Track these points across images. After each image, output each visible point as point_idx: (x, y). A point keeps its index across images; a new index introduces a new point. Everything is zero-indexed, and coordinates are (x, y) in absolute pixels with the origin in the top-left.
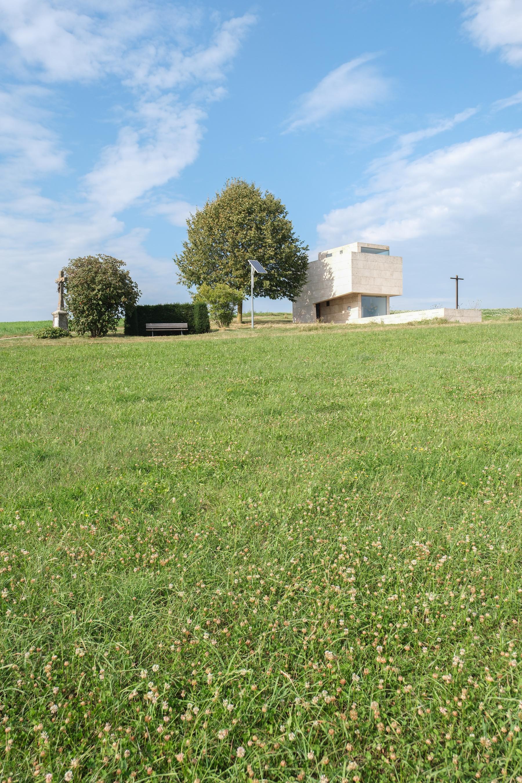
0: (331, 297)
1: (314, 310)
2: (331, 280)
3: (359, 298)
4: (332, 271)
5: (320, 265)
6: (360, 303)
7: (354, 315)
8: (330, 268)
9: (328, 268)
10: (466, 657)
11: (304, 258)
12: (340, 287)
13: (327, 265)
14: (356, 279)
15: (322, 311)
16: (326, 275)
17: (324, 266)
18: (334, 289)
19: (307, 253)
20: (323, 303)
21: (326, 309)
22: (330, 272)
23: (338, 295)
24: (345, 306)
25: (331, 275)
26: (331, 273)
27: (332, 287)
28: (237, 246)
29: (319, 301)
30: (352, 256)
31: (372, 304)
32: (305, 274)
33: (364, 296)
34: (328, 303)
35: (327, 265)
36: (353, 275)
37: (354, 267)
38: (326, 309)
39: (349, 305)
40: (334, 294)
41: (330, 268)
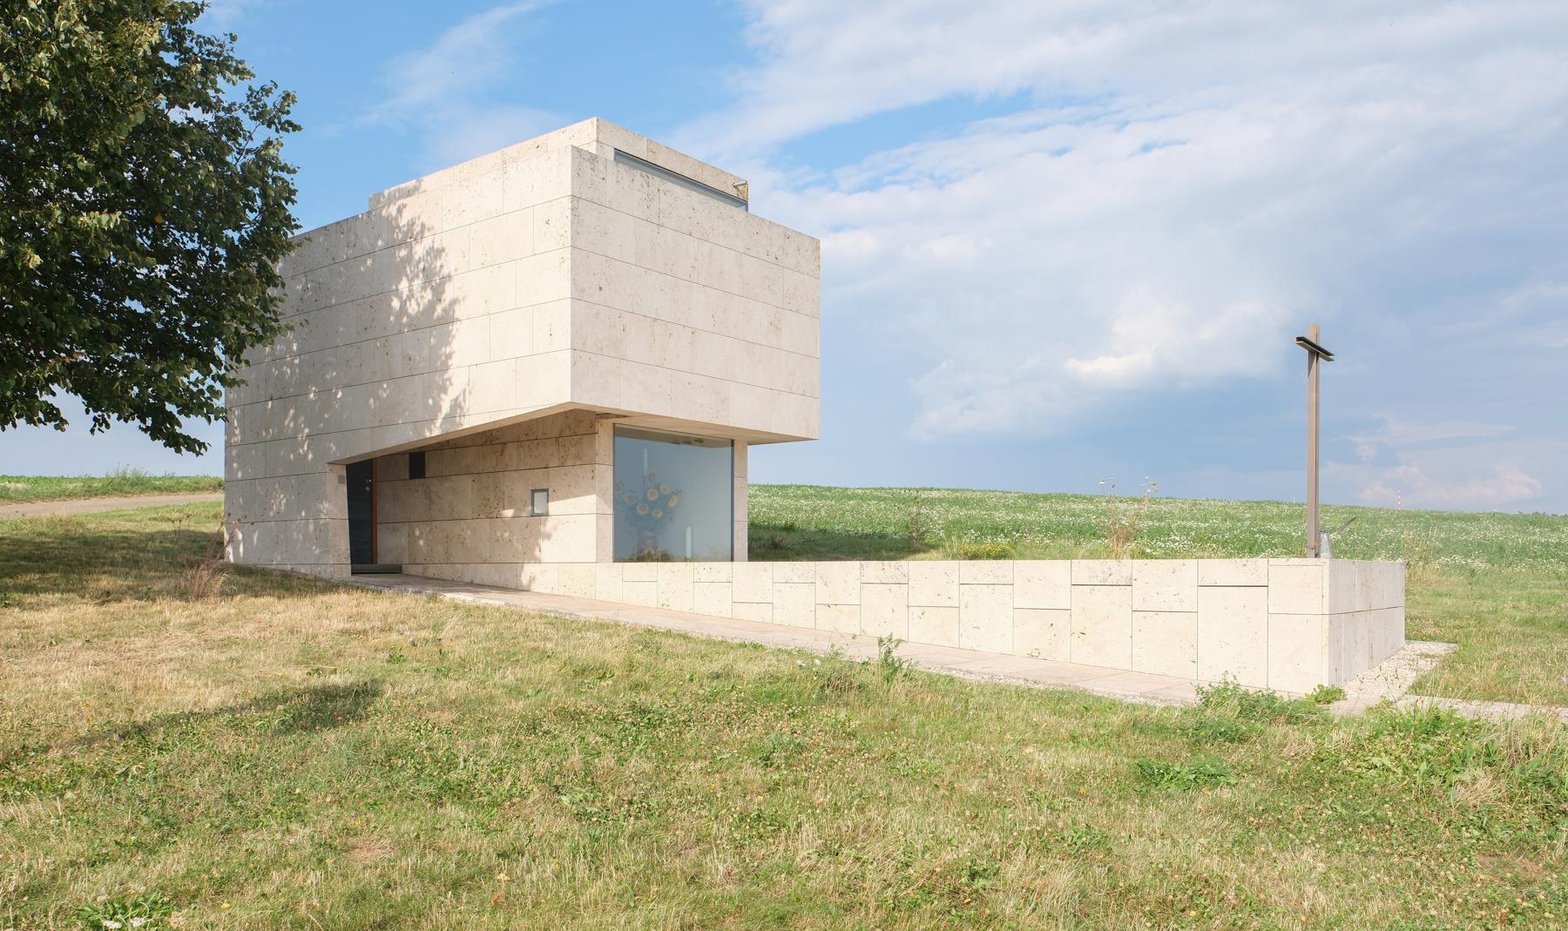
0: (435, 431)
1: (334, 507)
2: (437, 322)
3: (604, 441)
4: (448, 264)
5: (372, 243)
6: (606, 474)
7: (568, 550)
8: (436, 253)
9: (419, 250)
10: (24, 25)
11: (266, 186)
12: (496, 369)
13: (412, 235)
14: (596, 324)
15: (384, 507)
16: (410, 295)
17: (392, 246)
18: (458, 378)
19: (289, 150)
20: (391, 457)
21: (405, 501)
22: (428, 274)
23: (476, 417)
24: (516, 485)
25: (438, 293)
26: (436, 282)
29: (365, 446)
30: (577, 174)
31: (660, 479)
32: (271, 280)
33: (632, 433)
34: (418, 461)
35: (412, 235)
36: (578, 295)
38: (405, 501)
39: (537, 478)
41: (436, 253)
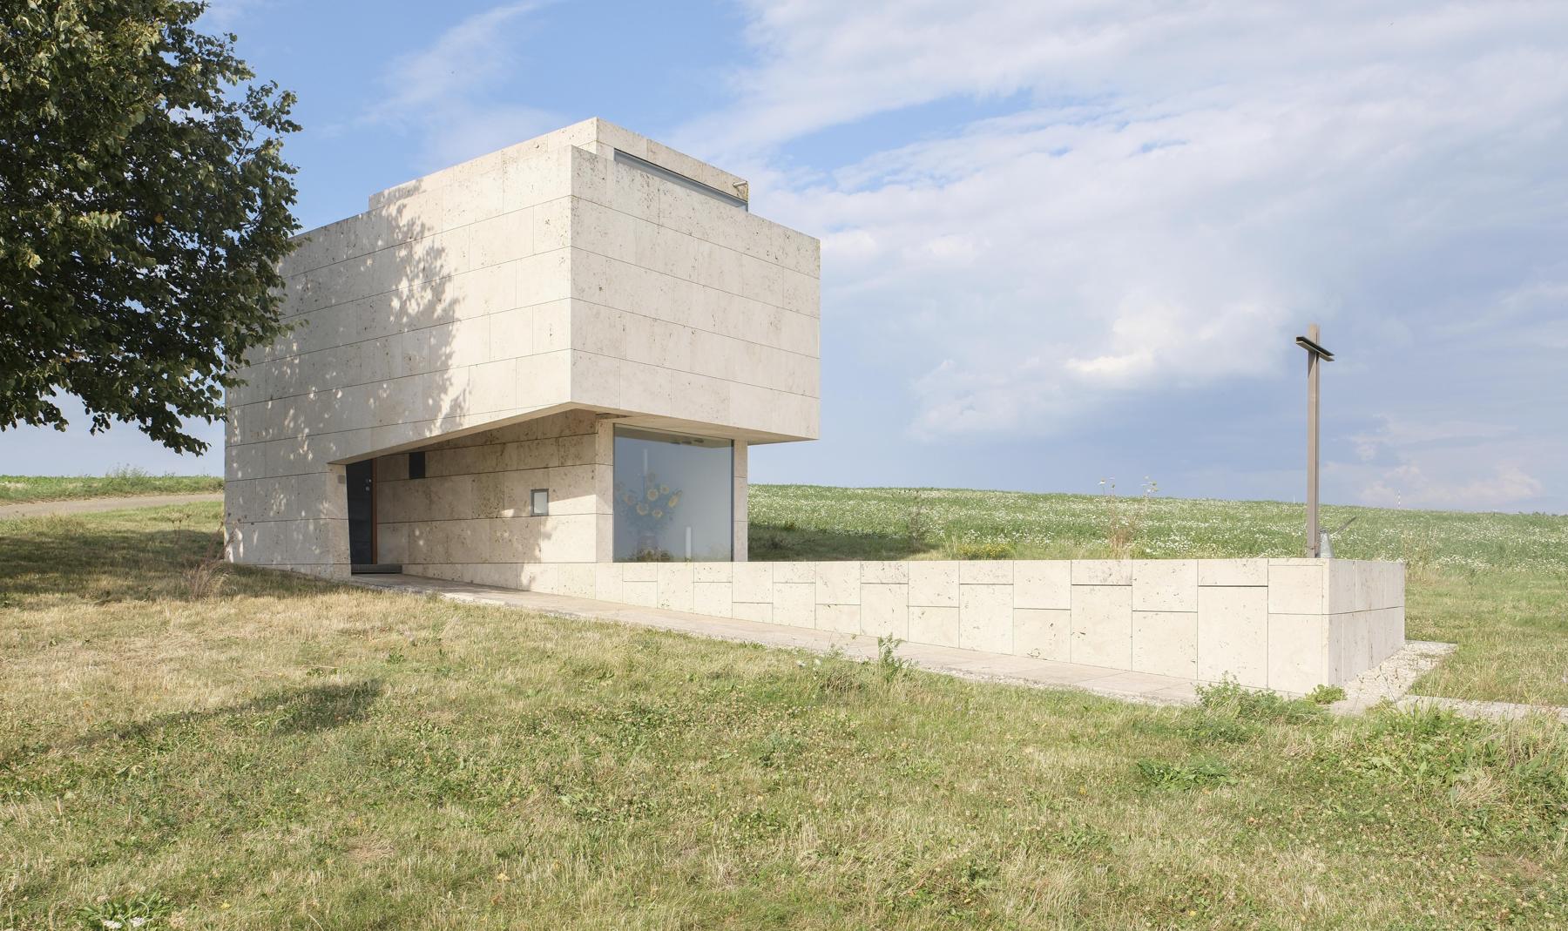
0: (435, 431)
1: (334, 506)
2: (438, 322)
3: (604, 442)
4: (449, 264)
5: (371, 243)
6: (606, 474)
9: (419, 250)
10: (24, 25)
11: (266, 186)
12: (497, 369)
13: (411, 236)
14: (596, 323)
15: (385, 506)
16: (410, 295)
17: (392, 246)
18: (458, 378)
19: (289, 150)
21: (407, 501)
22: (428, 274)
23: (476, 417)
24: (516, 485)
25: (438, 298)
26: (436, 282)
27: (445, 368)
28: (391, 660)
29: (366, 446)
30: (577, 173)
31: (660, 479)
32: (271, 280)
33: (632, 433)
34: (418, 461)
36: (578, 294)
37: (586, 254)
38: (407, 501)
39: (538, 478)
40: (456, 405)
41: (437, 253)
